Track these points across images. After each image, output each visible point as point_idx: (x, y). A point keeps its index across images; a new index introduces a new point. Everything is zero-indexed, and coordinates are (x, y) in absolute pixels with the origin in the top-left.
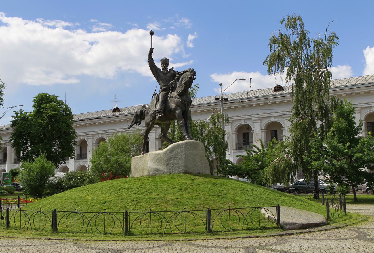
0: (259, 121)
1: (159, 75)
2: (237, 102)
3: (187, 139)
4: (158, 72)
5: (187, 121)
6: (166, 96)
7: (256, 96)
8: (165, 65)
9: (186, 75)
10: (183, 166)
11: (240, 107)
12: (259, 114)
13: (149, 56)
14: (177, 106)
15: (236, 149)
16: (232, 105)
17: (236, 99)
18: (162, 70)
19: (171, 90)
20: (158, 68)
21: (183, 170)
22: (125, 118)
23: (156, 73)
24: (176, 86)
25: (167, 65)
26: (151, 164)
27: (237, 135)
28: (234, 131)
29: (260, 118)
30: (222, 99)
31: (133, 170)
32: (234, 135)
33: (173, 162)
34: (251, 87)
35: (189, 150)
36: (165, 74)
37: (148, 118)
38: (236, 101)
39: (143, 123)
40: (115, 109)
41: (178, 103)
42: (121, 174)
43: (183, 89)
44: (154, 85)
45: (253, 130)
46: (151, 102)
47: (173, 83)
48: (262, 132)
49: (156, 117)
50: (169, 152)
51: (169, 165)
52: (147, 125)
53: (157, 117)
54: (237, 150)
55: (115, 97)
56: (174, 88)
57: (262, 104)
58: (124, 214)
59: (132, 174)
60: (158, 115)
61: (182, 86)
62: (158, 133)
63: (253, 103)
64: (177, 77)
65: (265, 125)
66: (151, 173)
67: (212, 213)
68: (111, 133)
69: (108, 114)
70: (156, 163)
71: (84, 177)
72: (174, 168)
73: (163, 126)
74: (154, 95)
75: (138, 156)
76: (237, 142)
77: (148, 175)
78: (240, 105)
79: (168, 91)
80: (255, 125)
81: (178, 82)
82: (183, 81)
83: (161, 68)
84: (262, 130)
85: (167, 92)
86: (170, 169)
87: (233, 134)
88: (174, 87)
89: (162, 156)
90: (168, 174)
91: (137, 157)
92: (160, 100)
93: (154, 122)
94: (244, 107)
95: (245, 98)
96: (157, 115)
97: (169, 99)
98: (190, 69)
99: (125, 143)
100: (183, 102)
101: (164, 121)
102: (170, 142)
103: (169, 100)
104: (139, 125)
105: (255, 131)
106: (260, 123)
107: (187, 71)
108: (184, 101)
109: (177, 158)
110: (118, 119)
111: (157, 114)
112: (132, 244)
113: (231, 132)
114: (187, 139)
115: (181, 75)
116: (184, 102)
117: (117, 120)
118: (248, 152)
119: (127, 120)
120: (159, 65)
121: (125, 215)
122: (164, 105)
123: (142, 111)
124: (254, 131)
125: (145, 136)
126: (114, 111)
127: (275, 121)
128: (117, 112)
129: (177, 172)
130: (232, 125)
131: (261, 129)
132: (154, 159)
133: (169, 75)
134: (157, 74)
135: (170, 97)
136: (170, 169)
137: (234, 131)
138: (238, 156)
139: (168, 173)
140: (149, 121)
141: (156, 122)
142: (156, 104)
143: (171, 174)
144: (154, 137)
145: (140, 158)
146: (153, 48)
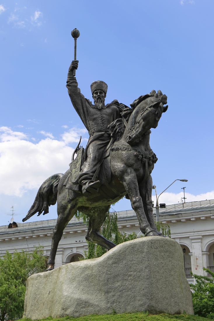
0: (200, 241)
1: (87, 111)
2: (170, 215)
3: (151, 234)
4: (87, 108)
5: (147, 200)
6: (102, 149)
7: (195, 208)
8: (100, 93)
9: (146, 103)
10: (144, 295)
11: (174, 221)
12: (199, 232)
13: (69, 74)
14: (128, 165)
16: (163, 219)
18: (93, 103)
19: (112, 139)
20: (86, 99)
21: (144, 304)
25: (103, 94)
26: (71, 291)
29: (200, 237)
30: (157, 205)
31: (29, 303)
33: (122, 285)
34: (184, 198)
35: (157, 259)
36: (100, 110)
37: (64, 196)
38: (169, 214)
39: (53, 209)
40: (12, 224)
41: (128, 159)
42: (13, 310)
43: (140, 130)
44: (77, 134)
45: (192, 253)
46: (71, 163)
47: (117, 124)
48: (203, 254)
49: (83, 188)
50: (110, 262)
51: (111, 292)
52: (61, 210)
53: (85, 187)
55: (12, 209)
56: (119, 134)
57: (204, 218)
59: (27, 313)
60: (88, 183)
61: (138, 125)
62: (66, 256)
63: (192, 217)
64: (124, 113)
65: (207, 245)
66: (68, 312)
69: (3, 230)
70: (82, 287)
72: (122, 300)
73: (94, 212)
74: (76, 151)
75: (42, 274)
77: (62, 316)
78: (174, 219)
79: (108, 141)
80: (194, 246)
83: (92, 100)
84: (204, 253)
86: (113, 302)
88: (118, 132)
90: (108, 314)
91: (40, 276)
93: (76, 204)
94: (179, 221)
95: (180, 211)
97: (107, 154)
99: (21, 266)
101: (96, 200)
102: (107, 246)
103: (108, 156)
104: (44, 214)
105: (194, 253)
106: (200, 243)
107: (147, 96)
108: (142, 155)
109: (130, 275)
110: (14, 236)
111: (84, 182)
114: (151, 234)
116: (143, 157)
117: (13, 237)
118: (199, 279)
119: (26, 237)
120: (87, 94)
122: (99, 165)
123: (52, 185)
124: (193, 254)
125: (55, 234)
126: (10, 226)
128: (14, 228)
129: (129, 308)
131: (202, 252)
132: (77, 279)
133: (108, 111)
134: (85, 109)
135: (111, 150)
136: (113, 302)
139: (110, 311)
140: (66, 201)
141: (79, 205)
143: (115, 313)
144: (61, 260)
145: (46, 276)
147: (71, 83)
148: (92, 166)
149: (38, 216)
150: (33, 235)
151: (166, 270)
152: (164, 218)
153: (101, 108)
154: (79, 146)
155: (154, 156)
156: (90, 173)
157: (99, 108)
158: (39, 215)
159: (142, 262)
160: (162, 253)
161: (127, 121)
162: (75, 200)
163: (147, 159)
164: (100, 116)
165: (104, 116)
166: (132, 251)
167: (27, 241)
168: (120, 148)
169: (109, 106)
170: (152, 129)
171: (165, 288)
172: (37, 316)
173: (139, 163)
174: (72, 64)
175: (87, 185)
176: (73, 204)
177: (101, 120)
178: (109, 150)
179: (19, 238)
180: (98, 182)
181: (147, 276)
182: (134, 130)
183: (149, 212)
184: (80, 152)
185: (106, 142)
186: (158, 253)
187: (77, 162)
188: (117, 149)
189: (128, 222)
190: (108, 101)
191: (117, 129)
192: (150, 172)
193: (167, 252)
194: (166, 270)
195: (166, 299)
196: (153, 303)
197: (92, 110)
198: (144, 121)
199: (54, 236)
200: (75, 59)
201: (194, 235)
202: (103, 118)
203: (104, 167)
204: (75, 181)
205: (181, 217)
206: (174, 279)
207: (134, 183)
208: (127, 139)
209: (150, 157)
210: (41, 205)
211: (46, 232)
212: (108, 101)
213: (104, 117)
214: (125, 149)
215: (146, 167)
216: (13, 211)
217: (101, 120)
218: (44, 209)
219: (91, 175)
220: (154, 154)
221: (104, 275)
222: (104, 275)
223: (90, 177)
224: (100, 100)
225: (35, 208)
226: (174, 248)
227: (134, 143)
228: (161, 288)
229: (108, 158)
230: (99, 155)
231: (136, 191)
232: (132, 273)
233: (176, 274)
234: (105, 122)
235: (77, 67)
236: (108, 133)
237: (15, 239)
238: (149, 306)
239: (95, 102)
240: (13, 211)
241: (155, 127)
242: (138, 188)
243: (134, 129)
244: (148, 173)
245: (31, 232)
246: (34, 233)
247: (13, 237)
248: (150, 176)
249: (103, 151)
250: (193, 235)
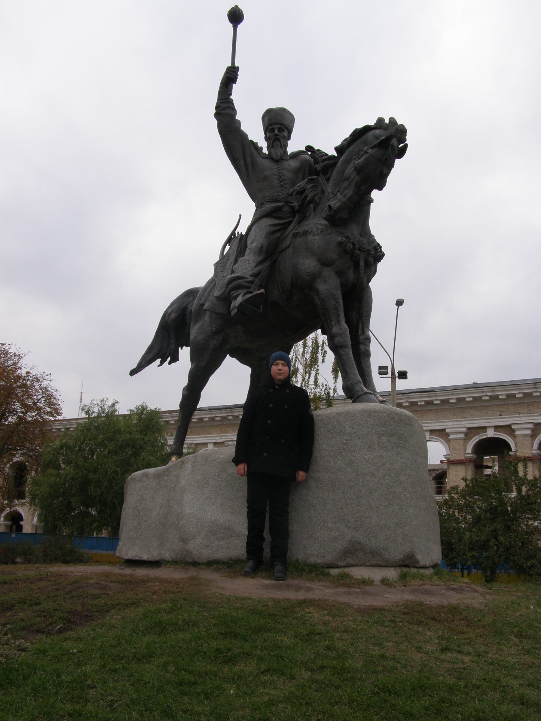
5: (360, 333)
6: (278, 234)
8: (280, 130)
9: (366, 143)
13: (220, 93)
18: (265, 151)
20: (251, 141)
23: (244, 155)
25: (286, 134)
43: (349, 193)
44: (232, 207)
47: (309, 186)
63: (451, 397)
71: (459, 494)
79: (290, 219)
83: (263, 144)
91: (146, 475)
103: (288, 246)
104: (170, 363)
108: (353, 244)
120: (255, 132)
122: (267, 264)
127: (495, 436)
133: (293, 164)
134: (249, 159)
145: (158, 476)
147: (224, 109)
148: (253, 265)
149: (159, 366)
151: (389, 472)
153: (279, 157)
154: (236, 232)
155: (378, 247)
156: (248, 277)
157: (275, 158)
158: (161, 365)
159: (341, 454)
160: (384, 438)
161: (328, 180)
163: (363, 253)
164: (277, 173)
165: (285, 172)
166: (323, 432)
168: (310, 230)
169: (296, 155)
170: (375, 194)
172: (137, 550)
175: (240, 299)
177: (278, 179)
178: (290, 236)
179: (170, 422)
180: (261, 293)
181: (349, 482)
182: (338, 194)
183: (363, 359)
184: (236, 243)
185: (285, 221)
187: (228, 260)
188: (305, 233)
190: (294, 145)
192: (369, 280)
194: (389, 472)
195: (386, 529)
197: (260, 160)
198: (358, 173)
201: (454, 426)
202: (282, 177)
204: (219, 294)
205: (433, 396)
207: (336, 299)
208: (325, 211)
209: (370, 250)
211: (215, 414)
212: (294, 145)
213: (283, 175)
214: (320, 230)
215: (360, 268)
217: (278, 179)
219: (249, 280)
220: (378, 244)
223: (247, 284)
224: (279, 143)
226: (408, 429)
227: (335, 220)
229: (288, 250)
231: (338, 315)
234: (285, 184)
235: (237, 78)
236: (290, 204)
238: (350, 541)
239: (268, 148)
241: (380, 188)
242: (341, 309)
243: (338, 191)
244: (365, 280)
248: (368, 287)
250: (451, 426)
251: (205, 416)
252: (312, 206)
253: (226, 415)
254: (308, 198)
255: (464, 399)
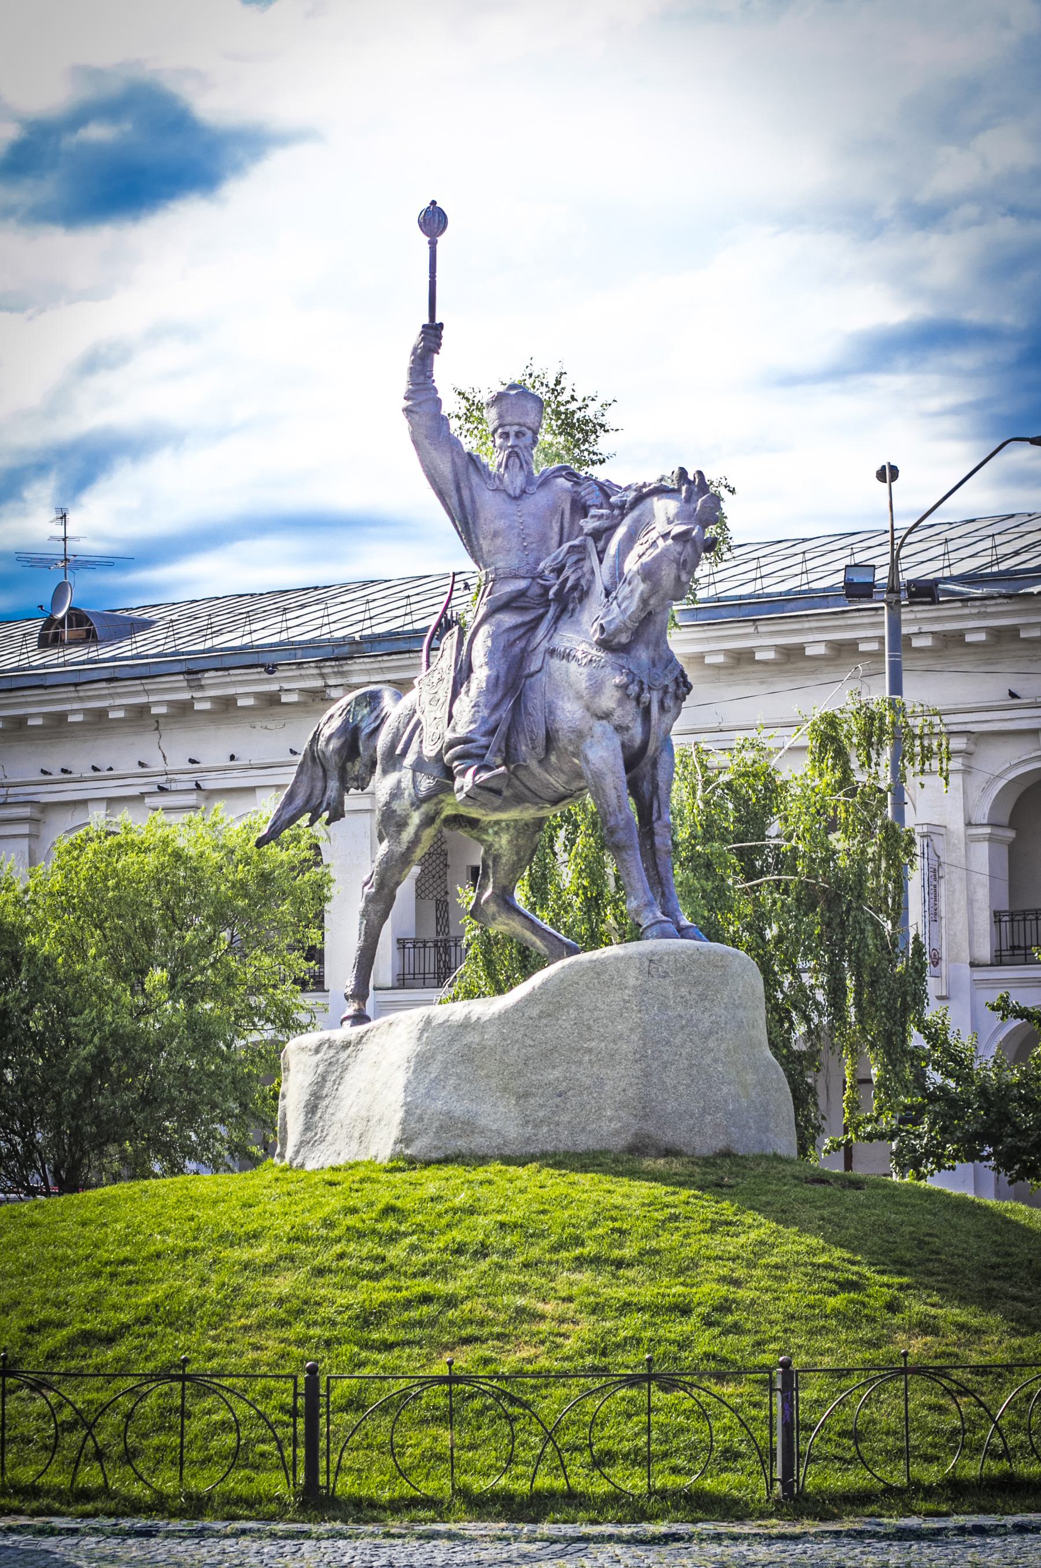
5: (654, 818)
6: (521, 644)
13: (412, 372)
15: (998, 960)
17: (1003, 566)
22: (142, 699)
24: (583, 582)
27: (1004, 851)
28: (985, 821)
32: (982, 852)
50: (535, 1012)
54: (1001, 964)
58: (296, 1385)
67: (923, 197)
68: (25, 812)
70: (954, 171)
72: (565, 1118)
73: (496, 833)
76: (1006, 907)
79: (541, 611)
81: (601, 554)
82: (638, 549)
85: (527, 617)
87: (971, 839)
88: (574, 588)
89: (490, 1036)
92: (481, 675)
93: (438, 813)
96: (463, 773)
98: (683, 472)
100: (634, 689)
108: (641, 683)
109: (590, 1051)
110: (81, 699)
112: (355, 1549)
113: (957, 825)
115: (623, 509)
119: (155, 710)
121: (301, 1389)
130: (967, 771)
132: (439, 1057)
137: (982, 814)
138: (1004, 1008)
142: (455, 694)
146: (438, 321)
150: (198, 694)
152: (975, 611)
153: (518, 492)
162: (435, 800)
167: (157, 729)
171: (688, 1086)
173: (631, 706)
174: (423, 339)
176: (427, 814)
186: (671, 988)
189: (761, 629)
191: (567, 579)
193: (697, 983)
196: (650, 1127)
199: (367, 906)
200: (433, 245)
202: (526, 531)
203: (526, 707)
206: (715, 1061)
210: (317, 792)
216: (65, 539)
217: (519, 535)
218: (328, 804)
221: (516, 1047)
222: (516, 1047)
225: (299, 801)
228: (675, 1087)
230: (509, 668)
232: (593, 1044)
233: (724, 1046)
237: (88, 718)
238: (636, 1134)
240: (65, 539)
245: (181, 677)
246: (201, 687)
247: (76, 706)
249: (524, 650)
251: (241, 690)
252: (576, 594)
253: (319, 683)
254: (569, 585)
255: (801, 648)
